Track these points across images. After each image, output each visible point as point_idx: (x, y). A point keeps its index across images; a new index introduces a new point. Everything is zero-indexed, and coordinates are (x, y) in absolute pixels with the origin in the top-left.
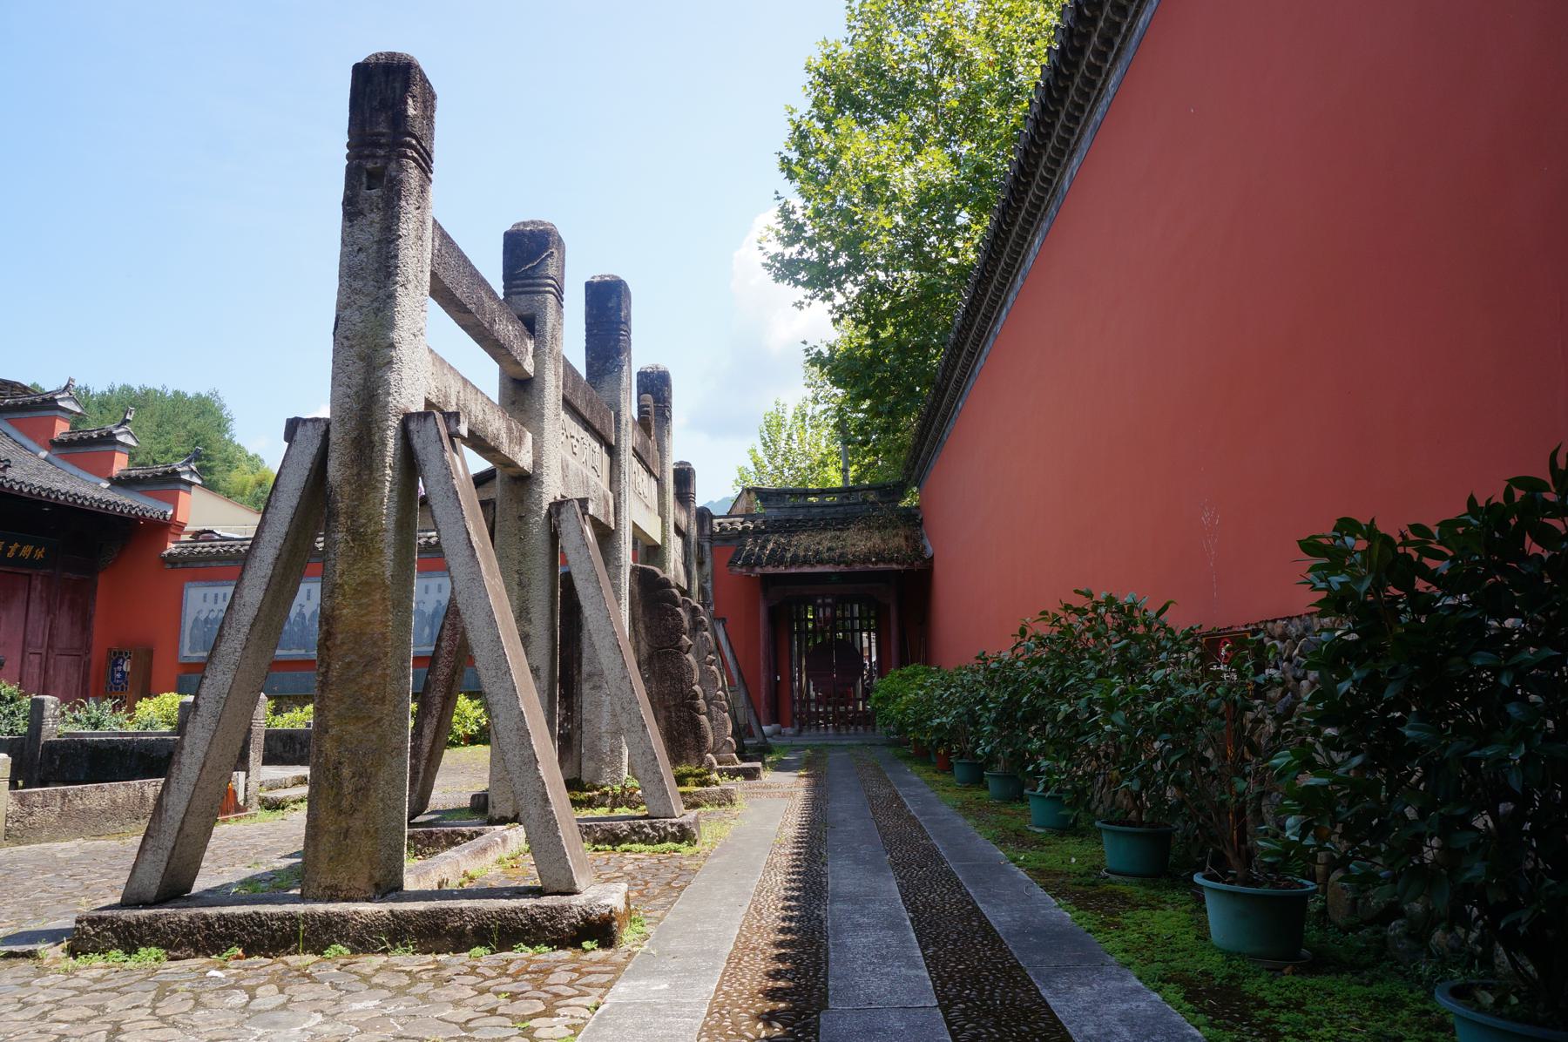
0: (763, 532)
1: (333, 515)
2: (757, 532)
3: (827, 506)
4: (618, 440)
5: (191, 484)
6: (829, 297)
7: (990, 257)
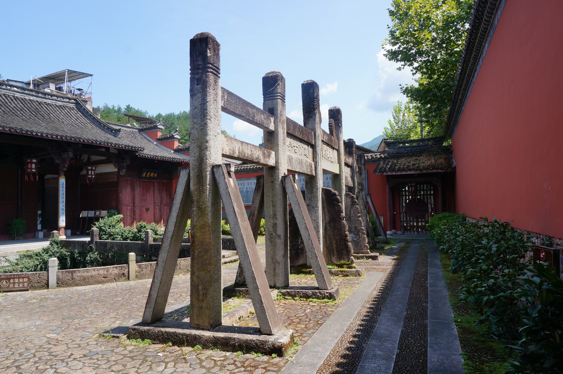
0: (388, 158)
1: (192, 202)
2: (385, 158)
3: (413, 147)
4: (315, 142)
6: (411, 65)
7: (467, 52)
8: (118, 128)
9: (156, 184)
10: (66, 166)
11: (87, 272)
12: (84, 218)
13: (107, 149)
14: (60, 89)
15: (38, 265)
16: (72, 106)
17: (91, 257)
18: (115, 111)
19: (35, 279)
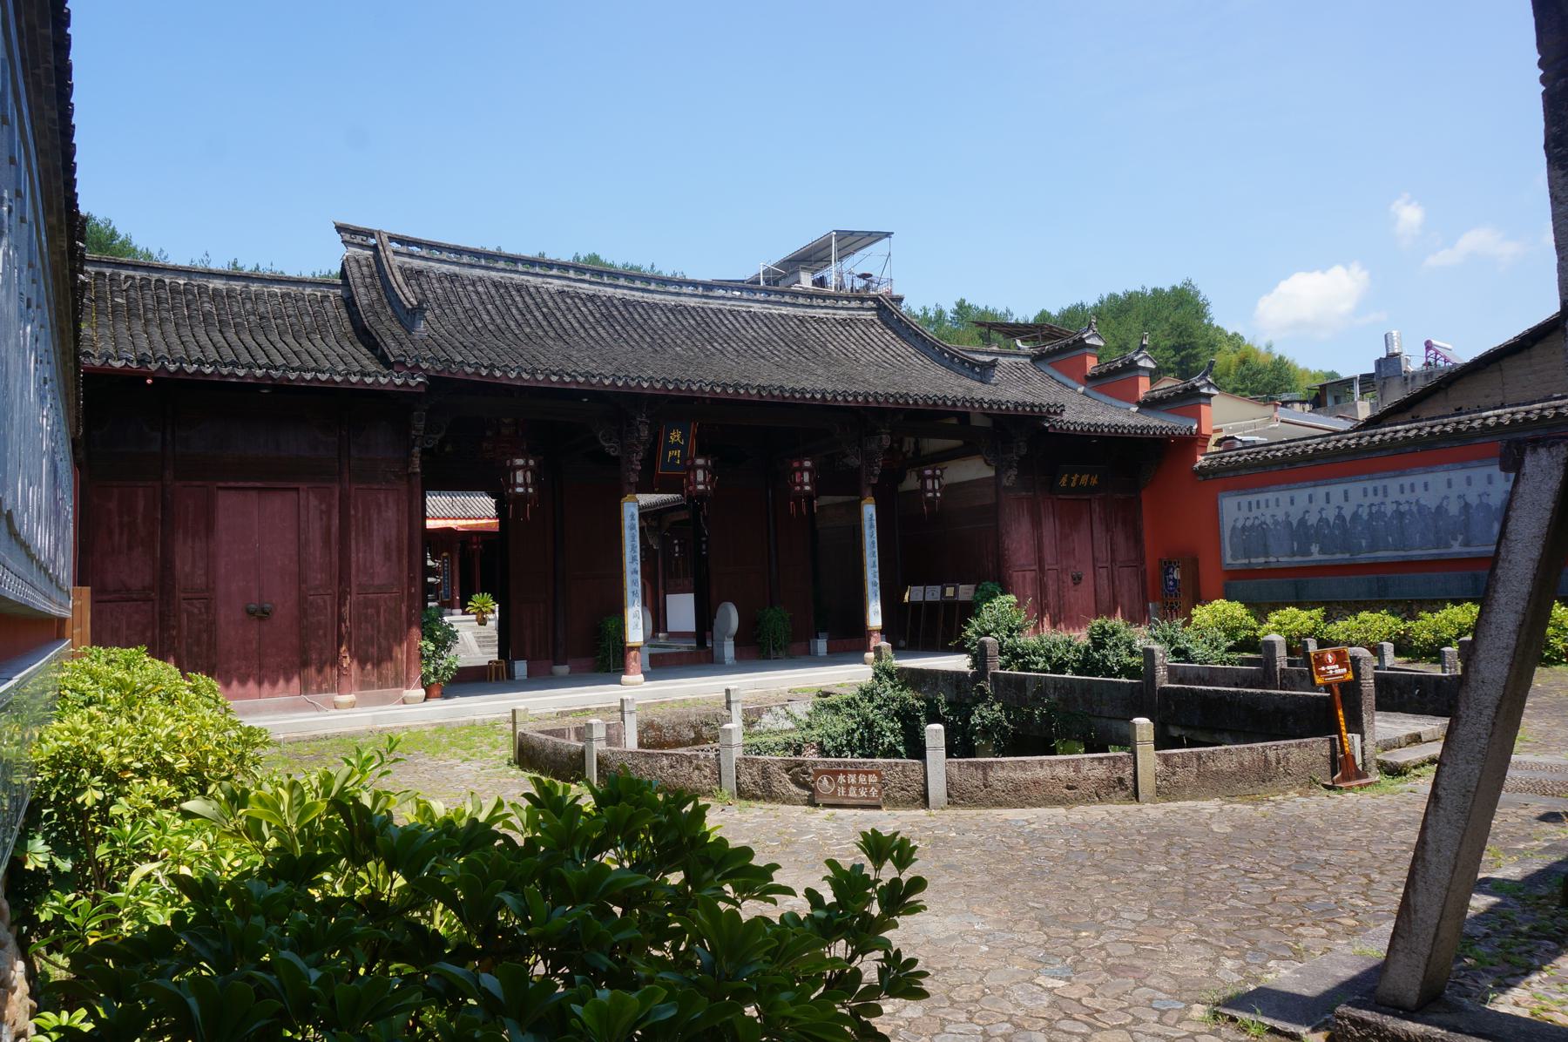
5: (1209, 396)
8: (988, 359)
9: (1096, 507)
10: (877, 471)
11: (1024, 770)
12: (915, 605)
13: (964, 417)
14: (821, 282)
15: (854, 731)
16: (869, 315)
17: (983, 718)
18: (930, 322)
19: (895, 778)
